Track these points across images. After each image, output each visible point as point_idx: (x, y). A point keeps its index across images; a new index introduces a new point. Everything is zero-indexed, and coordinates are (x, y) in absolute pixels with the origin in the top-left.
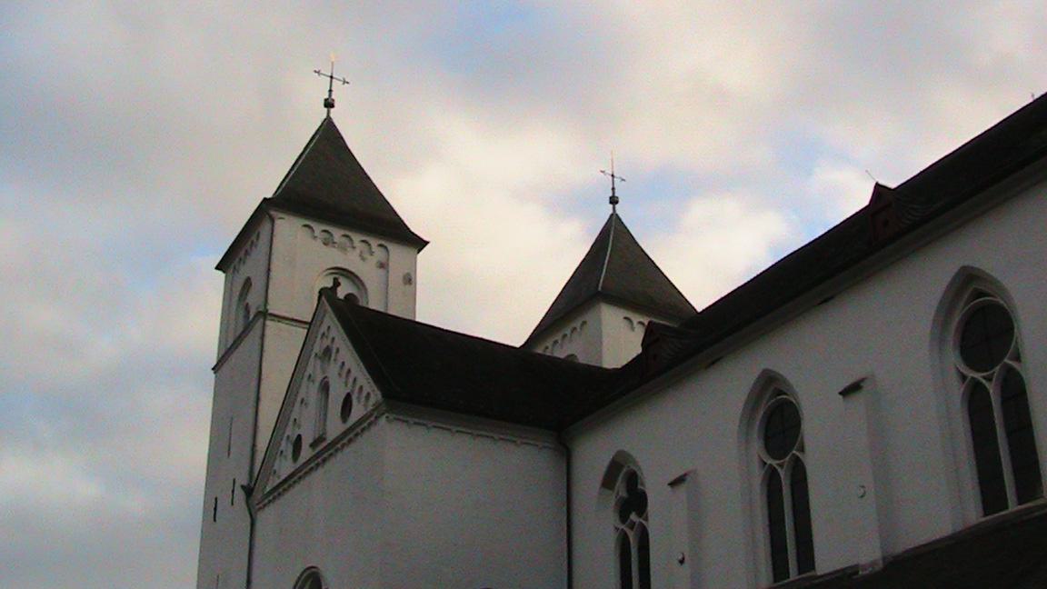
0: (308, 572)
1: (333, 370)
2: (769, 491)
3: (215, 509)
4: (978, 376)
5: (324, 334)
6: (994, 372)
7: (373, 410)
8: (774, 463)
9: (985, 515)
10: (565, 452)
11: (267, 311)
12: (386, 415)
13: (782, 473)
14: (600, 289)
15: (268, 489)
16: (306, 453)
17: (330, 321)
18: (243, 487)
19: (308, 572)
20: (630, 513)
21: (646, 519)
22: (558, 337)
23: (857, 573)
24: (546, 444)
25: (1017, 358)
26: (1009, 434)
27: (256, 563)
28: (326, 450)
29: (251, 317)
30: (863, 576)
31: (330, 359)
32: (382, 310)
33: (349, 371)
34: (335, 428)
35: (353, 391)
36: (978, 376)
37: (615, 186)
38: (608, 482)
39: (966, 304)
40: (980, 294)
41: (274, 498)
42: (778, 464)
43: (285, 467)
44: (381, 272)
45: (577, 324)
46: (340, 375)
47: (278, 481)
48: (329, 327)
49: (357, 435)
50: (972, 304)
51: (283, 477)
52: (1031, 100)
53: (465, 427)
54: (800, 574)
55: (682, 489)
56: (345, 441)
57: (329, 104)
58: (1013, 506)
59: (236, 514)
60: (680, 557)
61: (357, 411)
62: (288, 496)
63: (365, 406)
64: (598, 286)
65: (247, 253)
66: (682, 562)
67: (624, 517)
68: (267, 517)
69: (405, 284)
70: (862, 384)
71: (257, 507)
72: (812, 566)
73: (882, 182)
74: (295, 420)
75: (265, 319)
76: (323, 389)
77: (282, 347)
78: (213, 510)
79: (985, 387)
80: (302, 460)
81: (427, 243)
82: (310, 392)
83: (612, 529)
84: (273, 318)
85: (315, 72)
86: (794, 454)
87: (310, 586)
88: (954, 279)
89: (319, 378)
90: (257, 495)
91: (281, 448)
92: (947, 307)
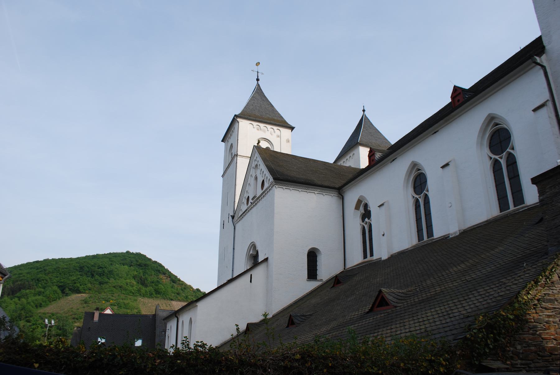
0: (252, 244)
1: (258, 172)
2: (415, 207)
3: (224, 224)
4: (497, 157)
6: (503, 155)
7: (271, 185)
8: (417, 196)
9: (501, 212)
11: (237, 154)
13: (420, 200)
14: (359, 141)
15: (239, 216)
16: (250, 201)
17: (257, 155)
18: (231, 216)
19: (252, 244)
20: (365, 218)
21: (371, 221)
22: (345, 160)
23: (449, 237)
24: (335, 195)
25: (513, 149)
26: (510, 179)
27: (236, 242)
28: (257, 199)
29: (233, 156)
30: (451, 238)
31: (257, 169)
32: (280, 152)
33: (263, 172)
34: (259, 192)
35: (264, 179)
36: (497, 157)
38: (357, 208)
39: (491, 128)
40: (497, 124)
41: (241, 219)
42: (419, 197)
43: (244, 207)
44: (279, 138)
45: (351, 154)
46: (260, 173)
48: (257, 157)
49: (266, 194)
50: (493, 129)
52: (520, 50)
53: (304, 189)
54: (428, 238)
55: (383, 207)
56: (262, 196)
57: (258, 80)
58: (512, 207)
59: (229, 225)
60: (383, 234)
61: (266, 185)
62: (245, 217)
63: (268, 183)
64: (358, 140)
65: (231, 135)
66: (383, 235)
67: (363, 220)
69: (287, 143)
70: (449, 163)
71: (236, 223)
72: (433, 236)
73: (457, 85)
74: (247, 191)
75: (237, 157)
76: (255, 179)
77: (242, 165)
78: (223, 225)
79: (499, 161)
80: (250, 204)
82: (251, 180)
84: (240, 156)
85: (252, 70)
86: (424, 193)
87: (253, 249)
88: (486, 117)
89: (254, 176)
90: (236, 218)
91: (243, 201)
92: (483, 130)
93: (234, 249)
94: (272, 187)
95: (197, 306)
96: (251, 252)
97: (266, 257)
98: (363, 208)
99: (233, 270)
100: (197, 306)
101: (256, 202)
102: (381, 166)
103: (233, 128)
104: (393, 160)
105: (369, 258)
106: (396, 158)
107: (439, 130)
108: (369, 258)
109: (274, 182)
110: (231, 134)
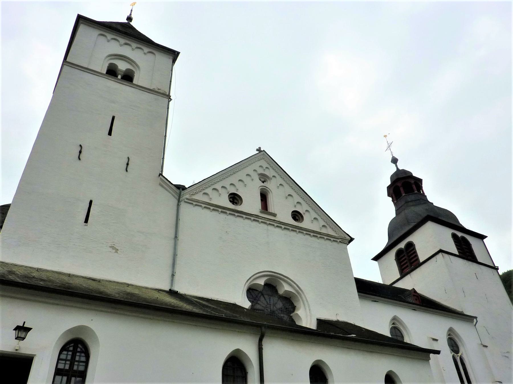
47: (205, 199)
93: (176, 237)
101: (291, 229)
104: (375, 301)
106: (378, 302)
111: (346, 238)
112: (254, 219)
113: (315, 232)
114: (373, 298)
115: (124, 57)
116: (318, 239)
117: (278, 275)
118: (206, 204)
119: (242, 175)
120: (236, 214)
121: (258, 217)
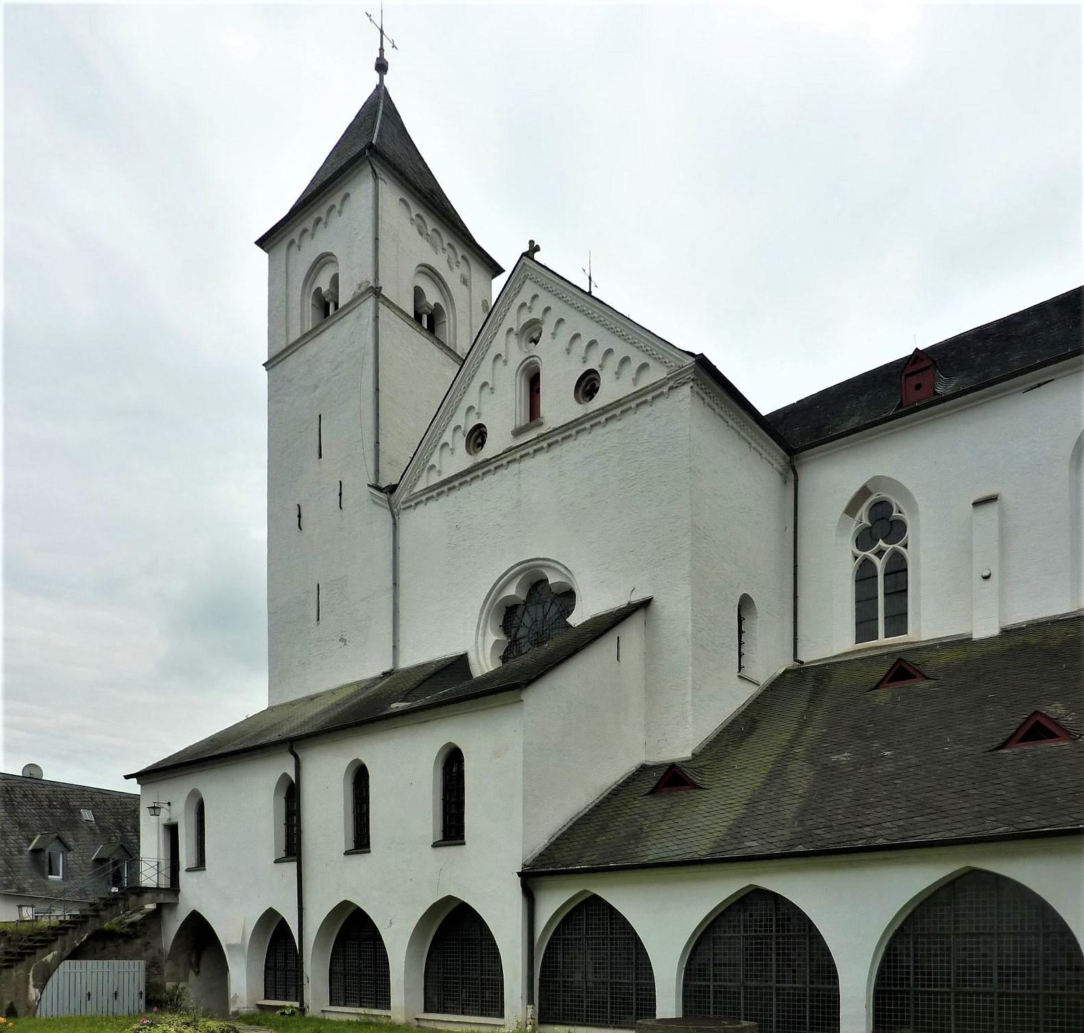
5: (523, 305)
10: (791, 473)
12: (691, 384)
27: (402, 557)
37: (298, 519)
38: (851, 509)
39: (856, 526)
43: (459, 460)
46: (568, 351)
47: (435, 479)
51: (444, 477)
55: (992, 509)
60: (986, 574)
66: (986, 578)
68: (413, 521)
80: (600, 401)
81: (504, 271)
83: (850, 558)
90: (402, 495)
93: (395, 584)
94: (671, 388)
95: (523, 701)
96: (511, 591)
97: (637, 597)
98: (867, 513)
99: (394, 647)
100: (523, 701)
101: (559, 438)
102: (965, 403)
103: (341, 194)
104: (1039, 385)
105: (882, 640)
106: (1053, 380)
107: (1057, 379)
108: (882, 640)
109: (693, 370)
110: (333, 207)
111: (683, 367)
112: (448, 489)
113: (608, 408)
114: (1020, 385)
115: (317, 263)
116: (620, 420)
117: (530, 563)
118: (424, 494)
119: (576, 322)
120: (468, 478)
121: (500, 458)
